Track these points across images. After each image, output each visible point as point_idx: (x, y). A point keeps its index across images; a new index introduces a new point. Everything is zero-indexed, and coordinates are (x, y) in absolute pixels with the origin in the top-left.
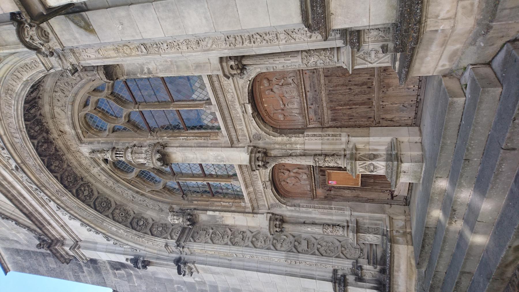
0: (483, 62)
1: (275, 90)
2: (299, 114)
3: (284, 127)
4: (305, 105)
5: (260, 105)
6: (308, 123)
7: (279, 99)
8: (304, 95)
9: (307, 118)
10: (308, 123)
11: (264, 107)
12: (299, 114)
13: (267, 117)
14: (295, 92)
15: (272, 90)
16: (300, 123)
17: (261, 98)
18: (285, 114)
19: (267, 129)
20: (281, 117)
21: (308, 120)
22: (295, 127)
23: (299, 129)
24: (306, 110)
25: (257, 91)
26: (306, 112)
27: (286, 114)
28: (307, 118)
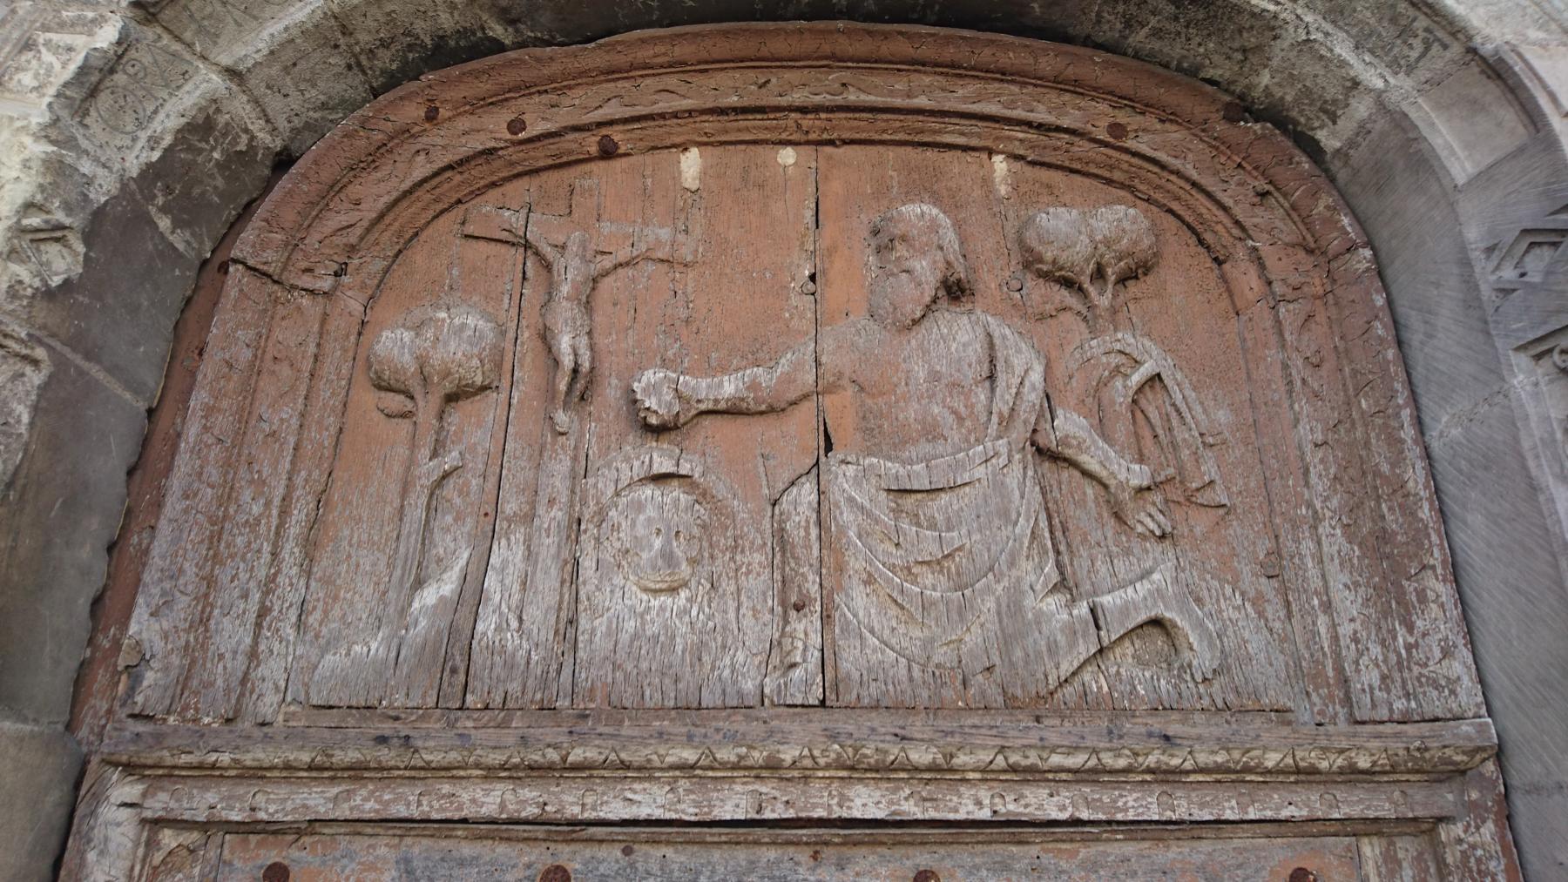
0: (1461, 557)
1: (958, 336)
2: (454, 654)
3: (231, 332)
4: (650, 801)
5: (732, 88)
6: (202, 802)
7: (788, 369)
8: (866, 802)
9: (317, 800)
10: (202, 802)
11: (662, 132)
12: (454, 654)
13: (493, 127)
14: (911, 637)
15: (955, 291)
16: (232, 634)
17: (824, 127)
18: (489, 409)
19: (285, 55)
20: (458, 333)
21: (275, 803)
22: (170, 543)
23: (108, 607)
24: (526, 799)
25: (963, 95)
26: (489, 800)
27: (475, 427)
28: (317, 800)
